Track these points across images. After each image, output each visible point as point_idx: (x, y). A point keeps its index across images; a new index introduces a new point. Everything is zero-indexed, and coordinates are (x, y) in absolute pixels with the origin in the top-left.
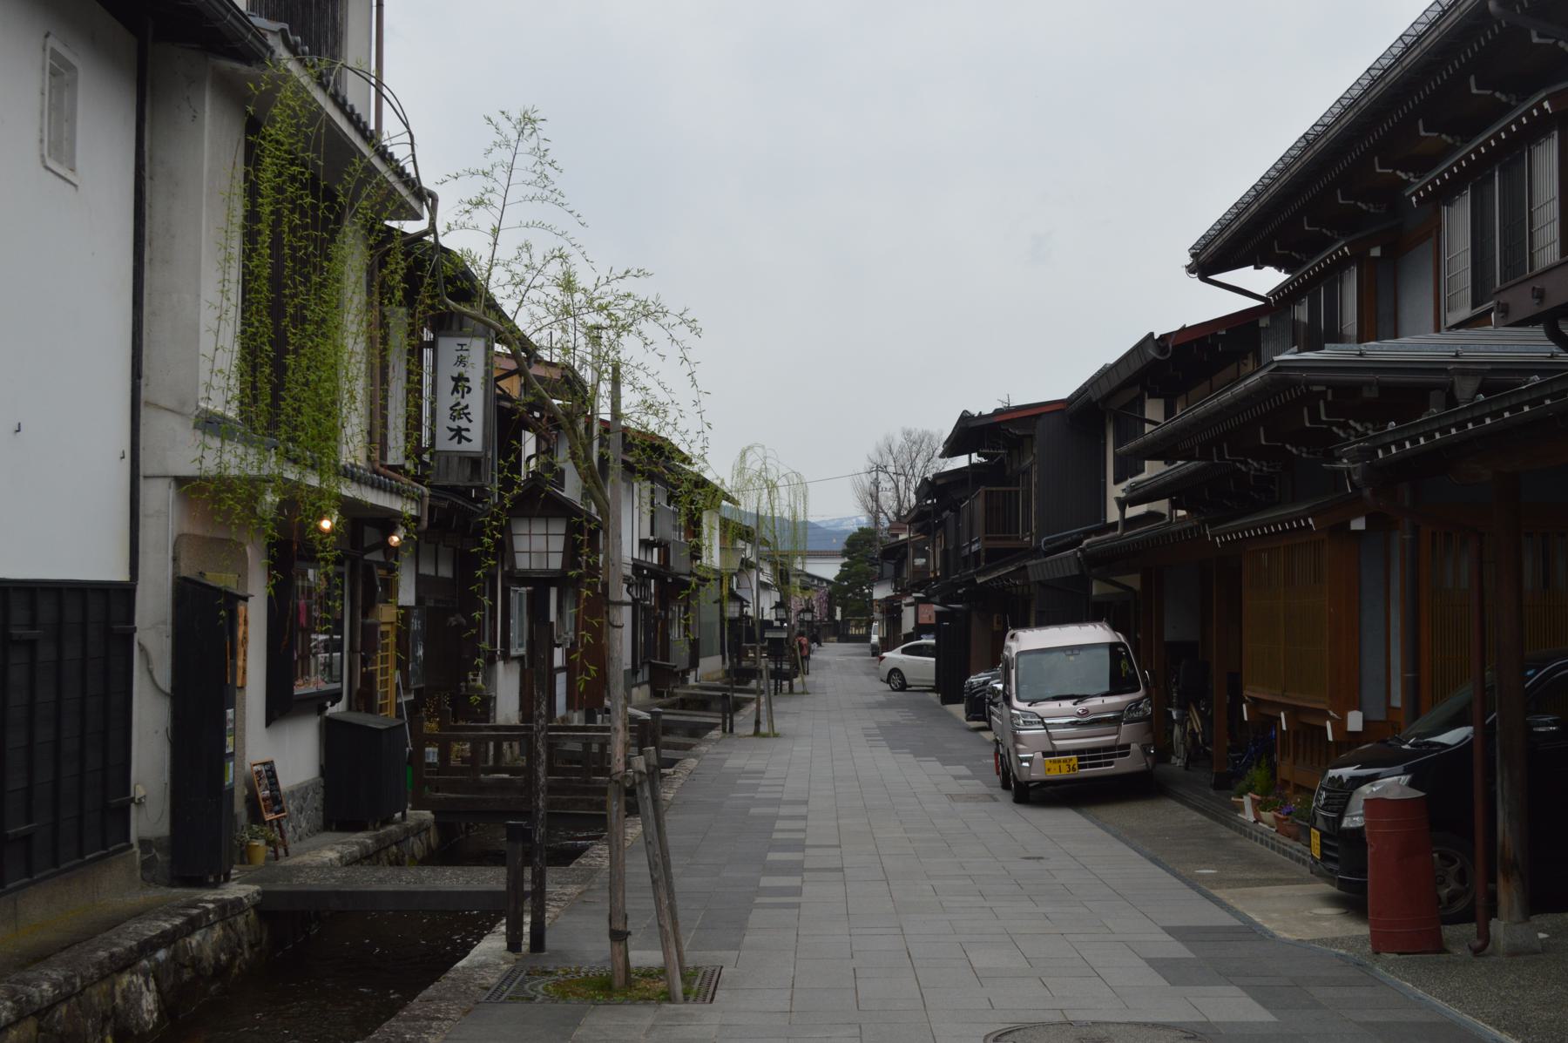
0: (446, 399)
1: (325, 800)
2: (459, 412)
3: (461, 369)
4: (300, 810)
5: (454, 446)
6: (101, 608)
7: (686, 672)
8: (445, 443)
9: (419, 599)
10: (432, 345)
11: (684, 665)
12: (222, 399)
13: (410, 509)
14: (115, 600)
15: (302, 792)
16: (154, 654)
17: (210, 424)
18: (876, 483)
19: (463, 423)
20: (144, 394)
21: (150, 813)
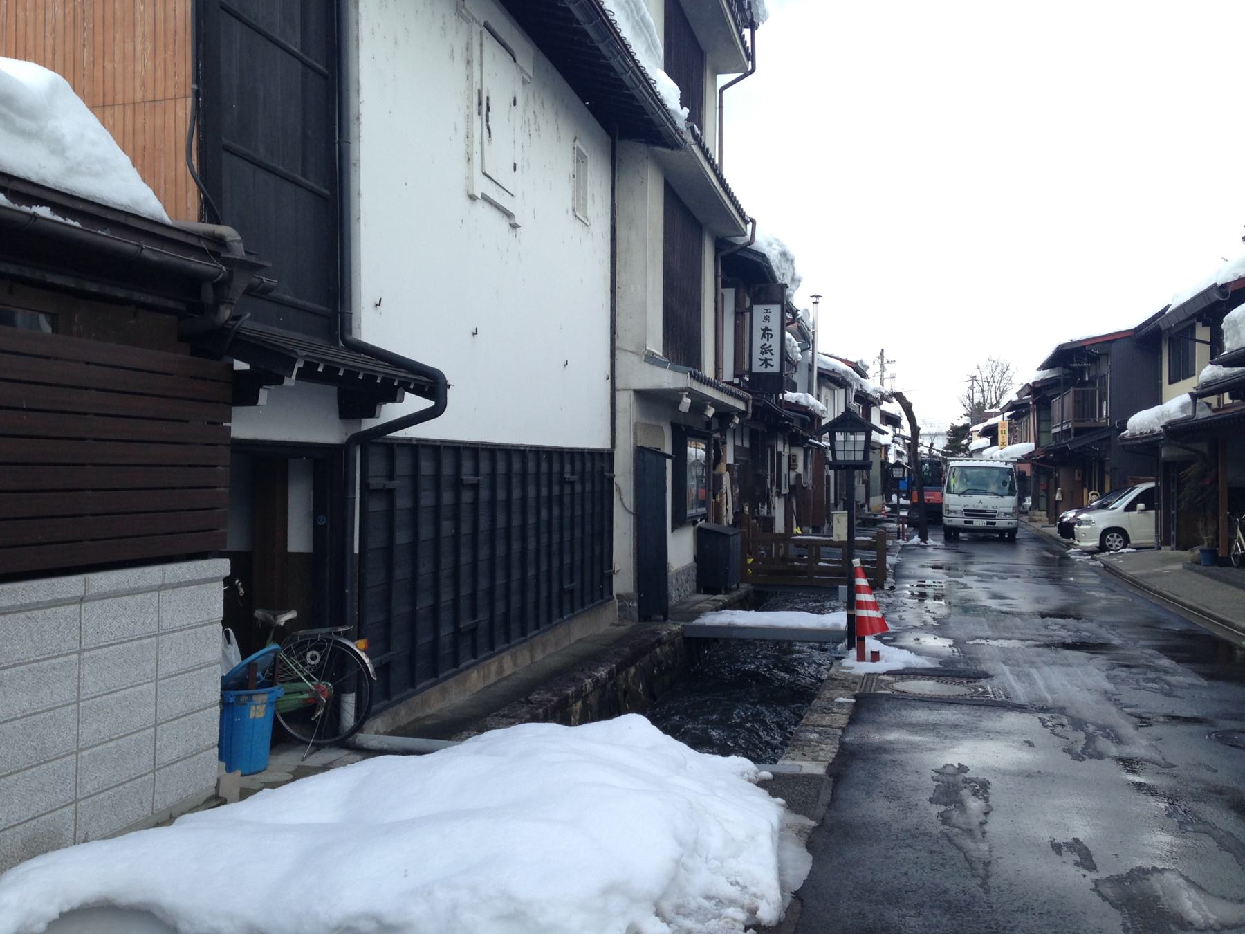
0: (758, 342)
1: (698, 576)
2: (765, 349)
3: (767, 324)
4: (687, 581)
5: (763, 369)
6: (591, 466)
7: (863, 506)
8: (757, 368)
9: (735, 461)
10: (750, 310)
11: (863, 501)
12: (655, 345)
13: (741, 406)
14: (604, 458)
15: (685, 571)
16: (623, 491)
17: (650, 358)
18: (972, 388)
19: (768, 356)
20: (617, 344)
21: (623, 581)
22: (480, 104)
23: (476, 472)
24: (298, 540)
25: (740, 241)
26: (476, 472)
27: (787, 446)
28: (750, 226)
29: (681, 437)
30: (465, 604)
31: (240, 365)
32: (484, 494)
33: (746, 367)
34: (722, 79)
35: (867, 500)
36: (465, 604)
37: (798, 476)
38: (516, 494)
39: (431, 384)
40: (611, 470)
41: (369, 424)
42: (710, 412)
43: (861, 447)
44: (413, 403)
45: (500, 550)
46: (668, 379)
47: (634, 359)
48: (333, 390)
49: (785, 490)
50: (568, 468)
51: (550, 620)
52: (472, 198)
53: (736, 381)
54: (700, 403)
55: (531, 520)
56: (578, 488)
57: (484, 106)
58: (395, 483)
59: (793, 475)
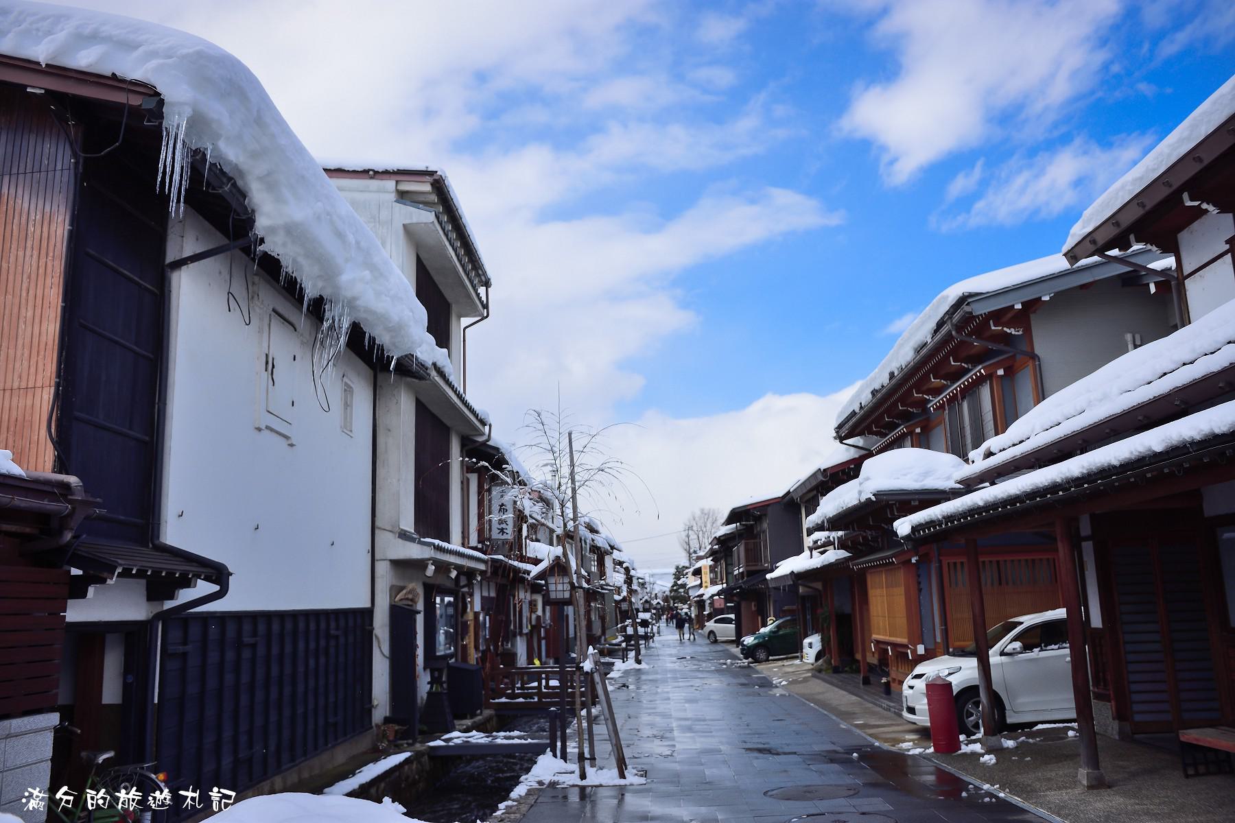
5: (501, 537)
10: (489, 490)
12: (408, 524)
14: (365, 615)
17: (404, 535)
19: (504, 526)
22: (267, 363)
23: (254, 634)
24: (111, 693)
25: (481, 439)
26: (254, 634)
27: (528, 595)
28: (487, 428)
29: (431, 590)
30: (243, 739)
31: (75, 572)
32: (261, 651)
33: (487, 535)
34: (465, 321)
35: (604, 633)
36: (243, 739)
37: (538, 617)
38: (288, 649)
39: (219, 574)
40: (371, 624)
41: (169, 604)
42: (454, 574)
43: (560, 596)
44: (204, 588)
45: (274, 695)
46: (414, 551)
47: (390, 535)
48: (144, 582)
49: (525, 631)
50: (333, 625)
51: (316, 748)
52: (259, 429)
53: (480, 546)
54: (442, 567)
55: (301, 669)
56: (342, 640)
57: (270, 365)
58: (189, 648)
59: (534, 616)
